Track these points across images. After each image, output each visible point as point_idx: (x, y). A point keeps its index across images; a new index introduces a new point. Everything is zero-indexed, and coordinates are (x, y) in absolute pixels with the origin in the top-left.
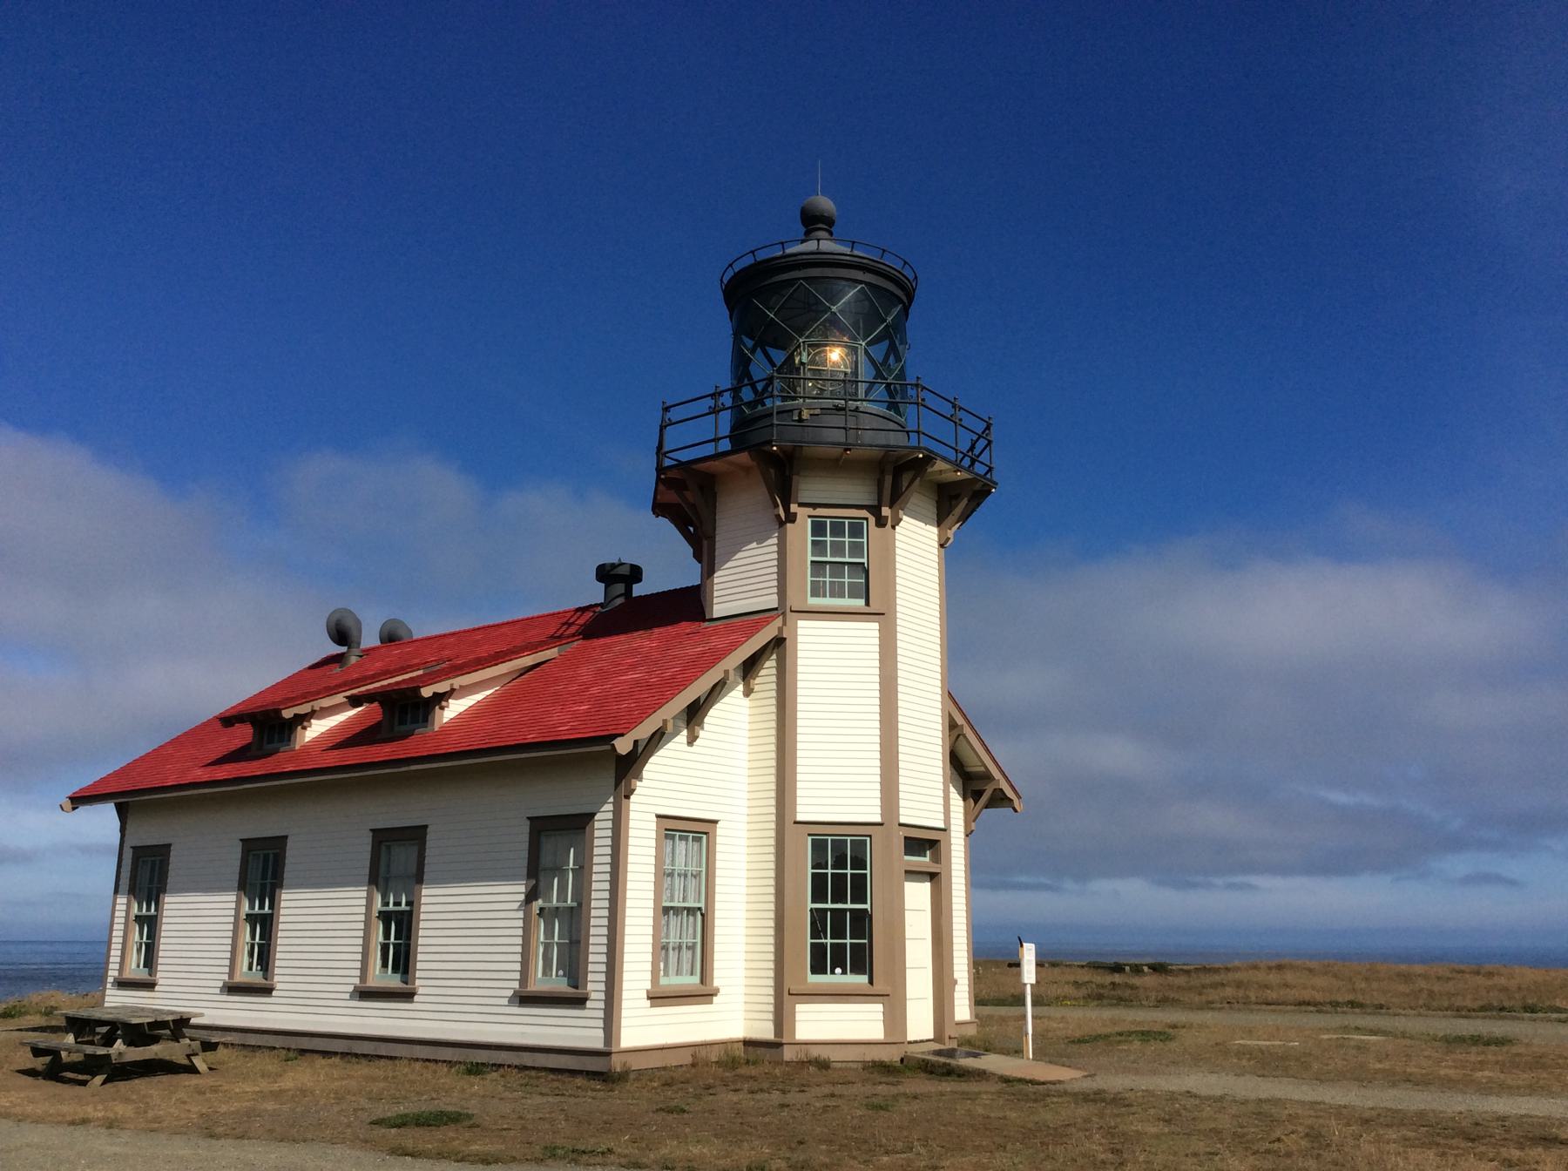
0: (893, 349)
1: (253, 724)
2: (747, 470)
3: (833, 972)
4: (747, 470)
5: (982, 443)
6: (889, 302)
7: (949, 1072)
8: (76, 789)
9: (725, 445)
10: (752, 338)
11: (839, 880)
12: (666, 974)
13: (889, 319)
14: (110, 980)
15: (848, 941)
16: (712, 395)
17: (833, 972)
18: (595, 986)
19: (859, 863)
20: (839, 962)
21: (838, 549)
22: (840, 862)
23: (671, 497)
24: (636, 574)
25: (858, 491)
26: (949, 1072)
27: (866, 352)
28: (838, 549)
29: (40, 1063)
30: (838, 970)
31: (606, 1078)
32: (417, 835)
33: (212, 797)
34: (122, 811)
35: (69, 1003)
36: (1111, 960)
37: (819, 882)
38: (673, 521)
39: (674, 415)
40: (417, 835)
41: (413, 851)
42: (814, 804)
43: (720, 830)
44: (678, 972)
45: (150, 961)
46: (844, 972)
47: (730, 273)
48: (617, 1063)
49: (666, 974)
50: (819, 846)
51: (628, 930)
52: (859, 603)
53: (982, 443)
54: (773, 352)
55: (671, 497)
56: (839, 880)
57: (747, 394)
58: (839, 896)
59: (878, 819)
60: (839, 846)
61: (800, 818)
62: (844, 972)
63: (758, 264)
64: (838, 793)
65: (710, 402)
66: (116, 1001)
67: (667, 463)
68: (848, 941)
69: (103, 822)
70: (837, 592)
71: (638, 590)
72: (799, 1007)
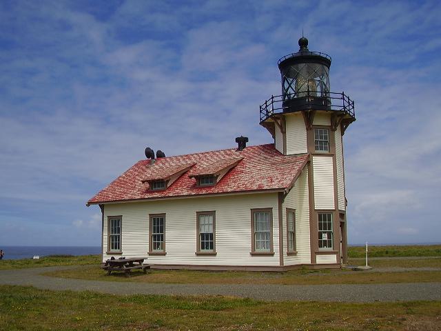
11: (325, 224)
19: (212, 239)
20: (325, 245)
21: (321, 138)
24: (246, 140)
25: (327, 123)
29: (107, 272)
31: (316, 271)
33: (206, 198)
34: (102, 207)
37: (320, 224)
40: (213, 213)
41: (211, 218)
42: (319, 206)
44: (116, 248)
45: (295, 249)
48: (316, 268)
49: (113, 248)
50: (320, 216)
52: (327, 152)
56: (325, 224)
58: (158, 236)
64: (325, 200)
69: (96, 215)
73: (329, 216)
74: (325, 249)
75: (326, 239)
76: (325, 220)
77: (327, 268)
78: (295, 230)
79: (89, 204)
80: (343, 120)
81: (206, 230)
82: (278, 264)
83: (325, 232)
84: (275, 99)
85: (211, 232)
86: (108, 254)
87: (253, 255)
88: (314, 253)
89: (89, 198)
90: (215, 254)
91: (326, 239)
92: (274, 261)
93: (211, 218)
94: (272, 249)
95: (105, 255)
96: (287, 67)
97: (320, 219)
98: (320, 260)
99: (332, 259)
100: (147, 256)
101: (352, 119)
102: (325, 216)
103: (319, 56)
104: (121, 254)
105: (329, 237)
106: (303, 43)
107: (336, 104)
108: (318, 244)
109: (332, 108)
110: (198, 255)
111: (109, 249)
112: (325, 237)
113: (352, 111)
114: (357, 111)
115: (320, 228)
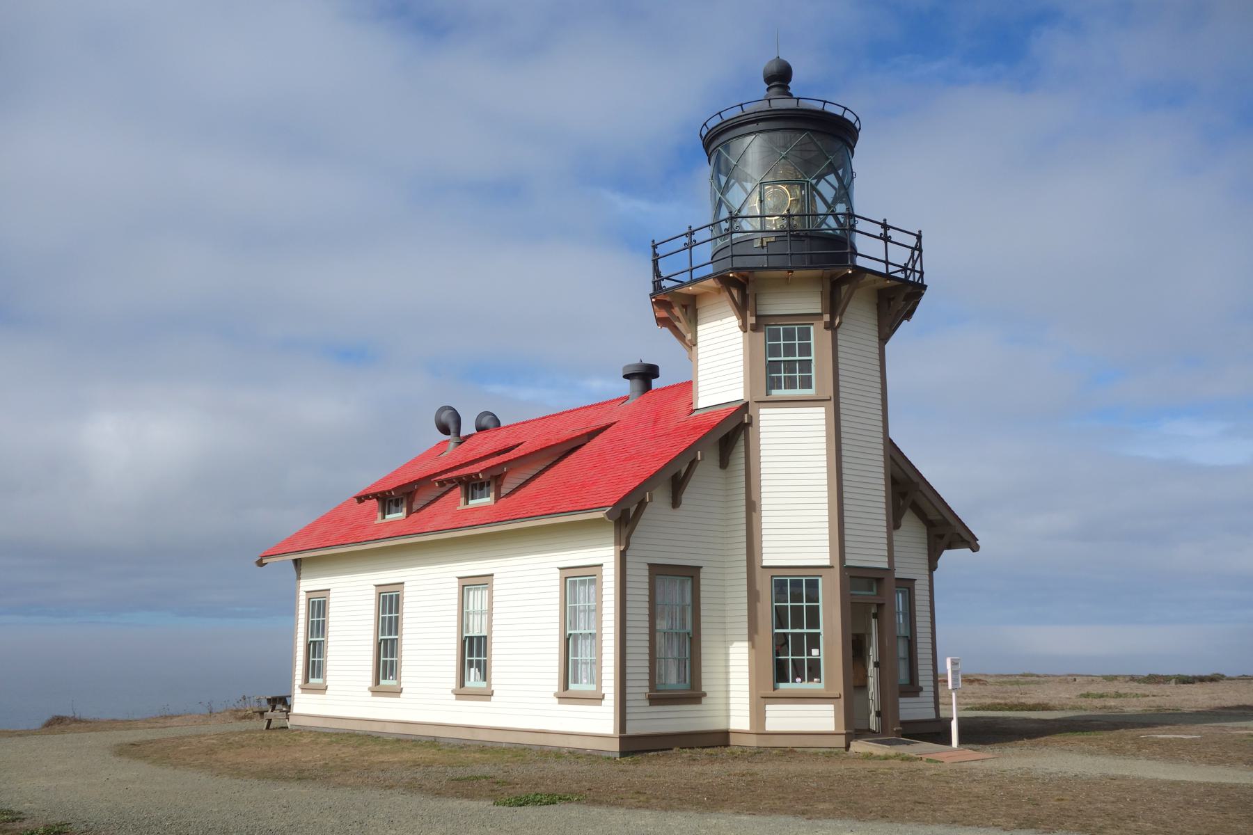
1: (378, 499)
3: (794, 681)
5: (916, 253)
6: (822, 137)
11: (797, 611)
16: (686, 235)
17: (794, 681)
18: (925, 679)
20: (798, 673)
21: (789, 350)
22: (797, 597)
23: (664, 314)
25: (810, 303)
28: (789, 350)
32: (484, 581)
36: (1146, 673)
41: (486, 593)
43: (703, 575)
46: (803, 680)
47: (704, 132)
50: (780, 586)
51: (557, 651)
53: (916, 253)
56: (797, 611)
58: (797, 623)
59: (827, 563)
60: (796, 584)
61: (765, 564)
62: (803, 680)
65: (686, 240)
70: (791, 384)
71: (656, 384)
72: (768, 707)
73: (813, 585)
77: (791, 748)
80: (898, 298)
82: (933, 716)
84: (698, 237)
93: (486, 593)
94: (600, 686)
95: (297, 693)
98: (787, 718)
99: (822, 718)
101: (925, 287)
106: (780, 77)
107: (869, 251)
109: (860, 262)
111: (306, 680)
113: (918, 267)
114: (933, 271)
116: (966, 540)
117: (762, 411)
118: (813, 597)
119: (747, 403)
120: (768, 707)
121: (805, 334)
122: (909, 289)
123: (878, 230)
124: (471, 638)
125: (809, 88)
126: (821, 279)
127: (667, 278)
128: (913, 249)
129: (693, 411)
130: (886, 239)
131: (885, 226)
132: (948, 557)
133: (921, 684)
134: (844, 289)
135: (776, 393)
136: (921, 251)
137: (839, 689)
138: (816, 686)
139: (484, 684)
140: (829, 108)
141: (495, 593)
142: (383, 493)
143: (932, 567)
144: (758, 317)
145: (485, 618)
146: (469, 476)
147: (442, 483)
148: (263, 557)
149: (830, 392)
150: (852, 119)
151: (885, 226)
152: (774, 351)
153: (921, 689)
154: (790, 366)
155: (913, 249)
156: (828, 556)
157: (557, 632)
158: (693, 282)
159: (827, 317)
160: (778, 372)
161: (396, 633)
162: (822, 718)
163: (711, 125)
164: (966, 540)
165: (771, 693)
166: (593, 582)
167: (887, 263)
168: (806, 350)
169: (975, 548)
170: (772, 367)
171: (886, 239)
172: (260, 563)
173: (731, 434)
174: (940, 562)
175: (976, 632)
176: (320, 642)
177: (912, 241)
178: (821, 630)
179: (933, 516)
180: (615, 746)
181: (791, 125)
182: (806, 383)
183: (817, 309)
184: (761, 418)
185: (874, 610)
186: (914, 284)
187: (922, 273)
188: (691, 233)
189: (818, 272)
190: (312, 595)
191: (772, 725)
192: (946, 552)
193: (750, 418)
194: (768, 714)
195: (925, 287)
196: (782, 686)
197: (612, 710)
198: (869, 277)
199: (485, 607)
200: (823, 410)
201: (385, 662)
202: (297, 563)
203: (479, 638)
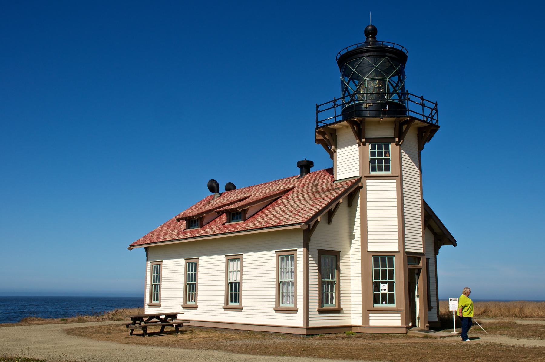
0: (400, 80)
2: (347, 127)
3: (382, 303)
4: (347, 127)
5: (434, 112)
6: (396, 59)
7: (249, 187)
8: (132, 243)
9: (340, 118)
10: (348, 77)
11: (384, 272)
12: (327, 302)
13: (397, 68)
14: (146, 305)
15: (377, 150)
17: (382, 303)
21: (380, 154)
23: (320, 137)
25: (388, 133)
26: (249, 187)
27: (389, 81)
28: (380, 154)
30: (384, 303)
35: (135, 312)
38: (322, 145)
39: (320, 108)
40: (296, 250)
44: (235, 302)
46: (386, 303)
47: (339, 56)
50: (376, 260)
54: (356, 81)
55: (320, 137)
56: (384, 272)
57: (348, 99)
59: (397, 250)
61: (369, 250)
62: (386, 303)
63: (348, 52)
66: (149, 311)
67: (320, 125)
68: (377, 150)
70: (380, 169)
72: (370, 315)
74: (384, 305)
75: (386, 292)
76: (384, 265)
78: (182, 219)
79: (178, 220)
81: (234, 278)
83: (385, 283)
85: (238, 280)
86: (150, 306)
87: (278, 310)
88: (367, 311)
89: (182, 213)
90: (240, 309)
91: (386, 292)
92: (296, 321)
93: (239, 262)
94: (296, 305)
95: (146, 307)
96: (367, 33)
97: (376, 265)
98: (377, 320)
99: (395, 320)
100: (181, 310)
101: (439, 127)
102: (383, 260)
103: (342, 56)
104: (456, 312)
105: (391, 288)
106: (372, 32)
107: (414, 109)
108: (375, 299)
110: (226, 309)
111: (151, 302)
112: (384, 288)
115: (377, 277)
116: (452, 241)
117: (367, 181)
118: (391, 264)
119: (361, 178)
120: (370, 315)
121: (387, 147)
122: (433, 128)
123: (420, 101)
124: (232, 283)
125: (384, 38)
126: (395, 122)
127: (320, 122)
128: (432, 110)
129: (334, 181)
130: (423, 105)
131: (422, 99)
132: (444, 249)
133: (432, 305)
134: (405, 127)
135: (373, 173)
136: (437, 111)
137: (403, 307)
138: (393, 306)
139: (194, 303)
140: (396, 47)
141: (243, 263)
142: (190, 217)
143: (436, 253)
144: (366, 139)
145: (239, 273)
146: (232, 209)
147: (218, 212)
148: (131, 246)
149: (398, 174)
150: (405, 52)
151: (422, 99)
152: (373, 154)
153: (432, 308)
154: (380, 161)
155: (432, 110)
156: (398, 247)
157: (224, 282)
158: (336, 123)
159: (397, 139)
160: (377, 164)
161: (195, 281)
162: (395, 320)
163: (342, 53)
164: (452, 241)
165: (371, 308)
166: (239, 259)
167: (423, 116)
168: (387, 153)
169: (455, 245)
170: (373, 161)
171: (423, 105)
172: (130, 249)
173: (353, 192)
174: (440, 251)
175: (459, 282)
176: (157, 285)
177: (433, 106)
178: (394, 280)
179: (437, 230)
180: (304, 332)
181: (375, 53)
182: (387, 169)
183: (392, 136)
184: (367, 184)
185: (416, 272)
186: (435, 125)
187: (437, 121)
188: (335, 100)
189: (393, 119)
190: (154, 263)
191: (372, 323)
192: (442, 247)
193: (362, 184)
194: (370, 318)
195: (439, 127)
196: (376, 305)
197: (302, 315)
198: (416, 121)
199: (239, 269)
200: (395, 181)
201: (154, 293)
202: (146, 249)
203: (236, 283)
